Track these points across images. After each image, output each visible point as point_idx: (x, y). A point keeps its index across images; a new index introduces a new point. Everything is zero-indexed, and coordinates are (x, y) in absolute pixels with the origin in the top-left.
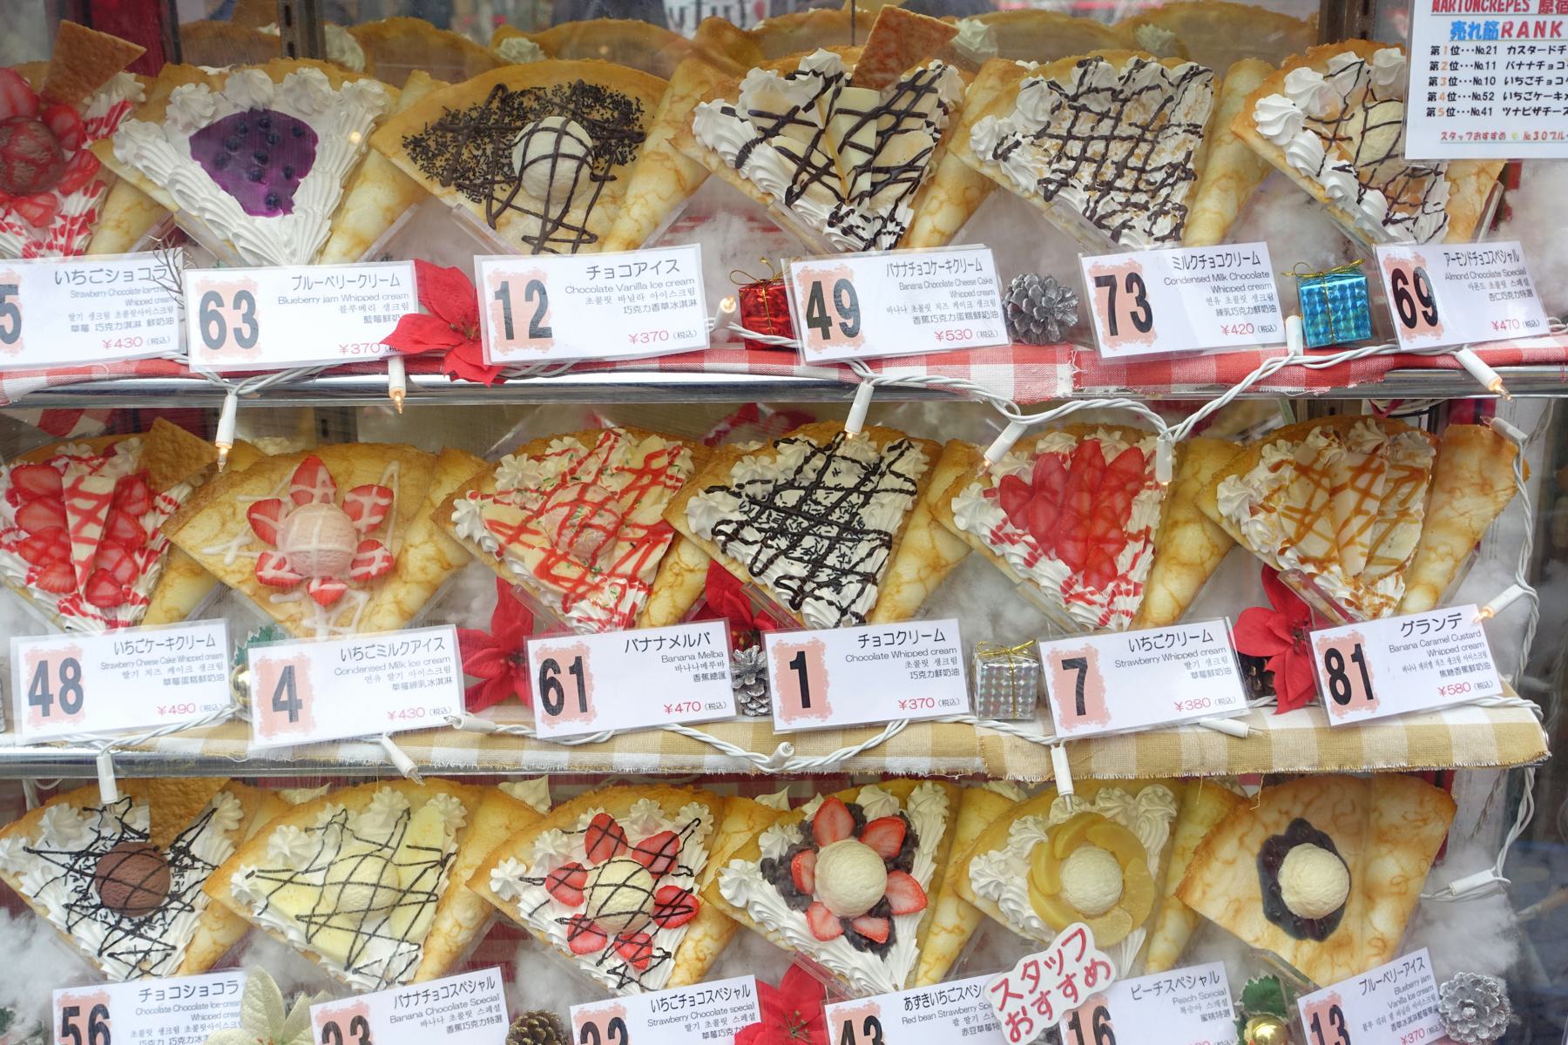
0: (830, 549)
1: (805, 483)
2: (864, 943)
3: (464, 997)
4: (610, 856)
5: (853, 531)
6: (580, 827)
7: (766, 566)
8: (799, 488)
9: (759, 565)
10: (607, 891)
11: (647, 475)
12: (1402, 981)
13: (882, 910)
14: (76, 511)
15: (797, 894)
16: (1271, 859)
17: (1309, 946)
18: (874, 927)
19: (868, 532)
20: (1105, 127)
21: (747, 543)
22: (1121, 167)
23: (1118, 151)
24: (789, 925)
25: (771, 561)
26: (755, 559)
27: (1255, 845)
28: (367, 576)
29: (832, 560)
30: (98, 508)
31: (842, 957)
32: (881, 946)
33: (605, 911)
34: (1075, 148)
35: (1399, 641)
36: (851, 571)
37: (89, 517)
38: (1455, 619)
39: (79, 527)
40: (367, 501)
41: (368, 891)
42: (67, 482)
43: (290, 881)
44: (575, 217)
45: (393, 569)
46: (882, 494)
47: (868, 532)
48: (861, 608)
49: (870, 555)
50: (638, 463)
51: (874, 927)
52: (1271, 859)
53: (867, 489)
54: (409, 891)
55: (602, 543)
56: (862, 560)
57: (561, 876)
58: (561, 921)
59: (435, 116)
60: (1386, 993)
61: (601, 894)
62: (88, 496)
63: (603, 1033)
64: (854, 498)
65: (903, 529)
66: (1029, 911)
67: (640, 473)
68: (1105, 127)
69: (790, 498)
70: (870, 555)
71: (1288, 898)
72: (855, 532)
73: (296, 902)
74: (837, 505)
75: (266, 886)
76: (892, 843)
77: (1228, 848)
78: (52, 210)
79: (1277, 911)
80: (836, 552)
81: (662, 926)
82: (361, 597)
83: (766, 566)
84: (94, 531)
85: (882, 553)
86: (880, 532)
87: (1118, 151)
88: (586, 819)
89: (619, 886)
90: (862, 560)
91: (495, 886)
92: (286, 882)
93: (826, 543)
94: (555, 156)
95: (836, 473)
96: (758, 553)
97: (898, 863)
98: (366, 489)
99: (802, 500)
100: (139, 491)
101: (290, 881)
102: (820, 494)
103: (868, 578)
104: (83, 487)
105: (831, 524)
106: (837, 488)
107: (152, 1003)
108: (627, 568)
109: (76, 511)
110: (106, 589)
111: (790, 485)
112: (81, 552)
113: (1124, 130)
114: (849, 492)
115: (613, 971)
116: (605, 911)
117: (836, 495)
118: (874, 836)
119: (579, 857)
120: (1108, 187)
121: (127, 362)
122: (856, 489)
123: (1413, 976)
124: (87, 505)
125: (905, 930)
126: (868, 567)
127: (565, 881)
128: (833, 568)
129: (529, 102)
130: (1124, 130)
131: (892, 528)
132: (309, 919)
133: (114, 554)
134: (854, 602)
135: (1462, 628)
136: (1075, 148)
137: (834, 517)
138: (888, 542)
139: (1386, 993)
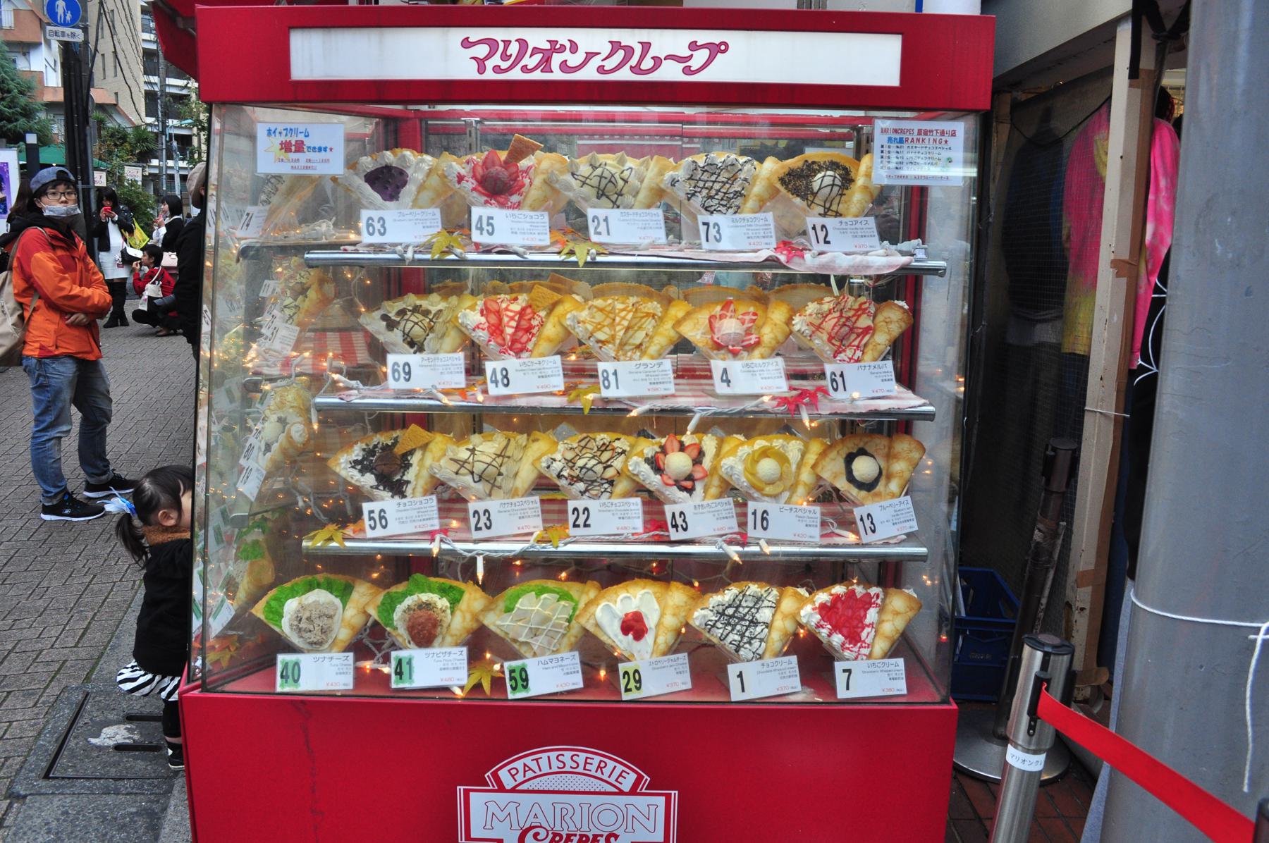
2: (683, 489)
3: (526, 506)
5: (754, 623)
11: (861, 311)
12: (898, 508)
13: (690, 478)
15: (658, 469)
16: (850, 459)
17: (863, 493)
18: (688, 484)
20: (713, 178)
22: (719, 191)
23: (717, 186)
24: (654, 481)
27: (844, 452)
28: (750, 345)
31: (674, 492)
32: (690, 491)
34: (701, 184)
35: (634, 369)
37: (512, 318)
38: (660, 365)
40: (747, 318)
42: (504, 305)
44: (834, 207)
45: (758, 343)
50: (856, 307)
51: (688, 484)
52: (850, 459)
55: (846, 336)
59: (786, 171)
60: (890, 511)
63: (481, 513)
66: (743, 479)
67: (857, 310)
68: (713, 178)
71: (856, 474)
76: (695, 453)
77: (833, 454)
78: (507, 200)
79: (851, 478)
82: (745, 354)
84: (514, 324)
85: (766, 630)
87: (717, 186)
94: (833, 185)
97: (697, 461)
98: (747, 313)
100: (529, 311)
103: (761, 640)
107: (402, 507)
108: (856, 343)
110: (518, 346)
111: (730, 606)
112: (509, 331)
113: (721, 179)
118: (689, 450)
120: (712, 198)
121: (890, 267)
123: (902, 507)
124: (511, 314)
125: (699, 487)
129: (816, 167)
130: (721, 179)
133: (520, 334)
135: (662, 368)
136: (701, 184)
138: (768, 625)
139: (890, 511)
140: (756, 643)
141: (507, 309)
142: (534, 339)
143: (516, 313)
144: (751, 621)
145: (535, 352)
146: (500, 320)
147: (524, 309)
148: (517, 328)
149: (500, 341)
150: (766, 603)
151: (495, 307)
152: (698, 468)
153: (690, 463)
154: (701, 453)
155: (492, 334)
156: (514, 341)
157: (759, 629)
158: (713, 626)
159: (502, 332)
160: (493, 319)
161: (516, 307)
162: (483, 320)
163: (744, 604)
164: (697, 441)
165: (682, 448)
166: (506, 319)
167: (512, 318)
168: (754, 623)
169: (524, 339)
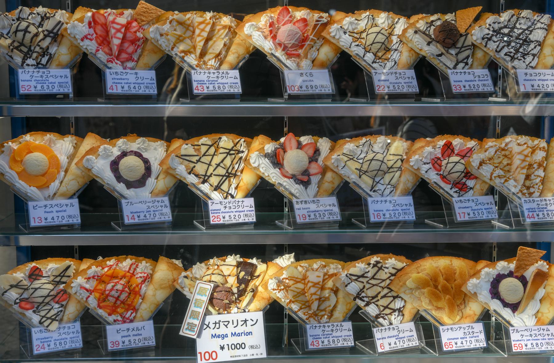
0: (520, 47)
1: (510, 26)
4: (449, 156)
5: (527, 42)
6: (438, 146)
7: (501, 49)
8: (508, 28)
9: (500, 48)
10: (453, 165)
13: (306, 172)
14: (114, 28)
19: (533, 42)
21: (494, 42)
25: (503, 47)
26: (498, 47)
29: (521, 50)
30: (121, 28)
33: (451, 172)
36: (528, 54)
37: (118, 31)
39: (115, 33)
41: (380, 163)
43: (352, 159)
46: (537, 30)
47: (533, 42)
48: (533, 64)
49: (535, 47)
51: (305, 178)
53: (531, 29)
54: (391, 167)
56: (532, 49)
57: (436, 160)
58: (437, 174)
61: (450, 166)
62: (118, 24)
64: (526, 32)
65: (544, 41)
69: (506, 31)
70: (535, 47)
72: (528, 42)
73: (353, 165)
74: (522, 33)
75: (346, 159)
76: (311, 152)
80: (522, 48)
81: (468, 179)
83: (501, 49)
84: (120, 35)
85: (538, 48)
86: (537, 41)
88: (441, 143)
89: (457, 163)
90: (532, 49)
91: (333, 161)
92: (351, 159)
93: (519, 45)
95: (520, 24)
96: (499, 44)
99: (510, 32)
100: (135, 24)
101: (352, 159)
102: (516, 30)
103: (534, 55)
104: (117, 21)
105: (520, 39)
106: (521, 29)
109: (114, 28)
111: (505, 27)
112: (116, 42)
114: (525, 30)
115: (456, 192)
116: (451, 172)
117: (521, 31)
118: (306, 149)
119: (440, 156)
122: (527, 29)
124: (118, 27)
126: (535, 52)
127: (436, 163)
128: (522, 53)
131: (541, 40)
132: (360, 170)
134: (530, 62)
137: (521, 37)
138: (541, 44)
140: (529, 59)
141: (113, 22)
142: (139, 51)
143: (123, 26)
144: (525, 40)
145: (141, 62)
146: (107, 32)
147: (129, 23)
148: (124, 39)
149: (106, 50)
150: (539, 25)
151: (102, 20)
152: (313, 165)
153: (306, 160)
154: (317, 151)
155: (100, 45)
156: (121, 50)
157: (532, 46)
158: (489, 39)
159: (109, 43)
160: (99, 29)
161: (122, 20)
162: (92, 31)
163: (518, 26)
164: (313, 141)
165: (300, 146)
166: (113, 31)
167: (118, 31)
168: (527, 42)
169: (131, 49)
